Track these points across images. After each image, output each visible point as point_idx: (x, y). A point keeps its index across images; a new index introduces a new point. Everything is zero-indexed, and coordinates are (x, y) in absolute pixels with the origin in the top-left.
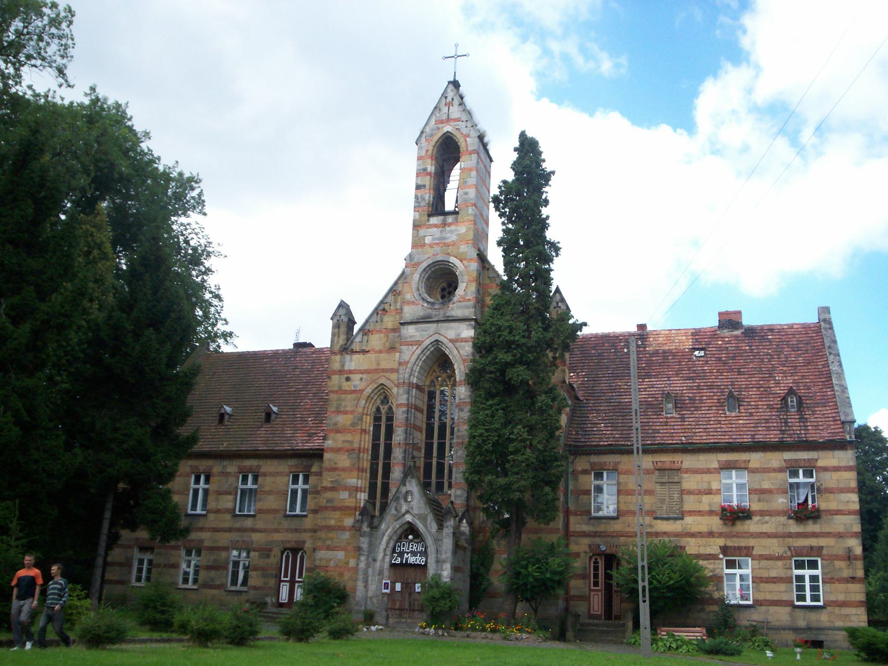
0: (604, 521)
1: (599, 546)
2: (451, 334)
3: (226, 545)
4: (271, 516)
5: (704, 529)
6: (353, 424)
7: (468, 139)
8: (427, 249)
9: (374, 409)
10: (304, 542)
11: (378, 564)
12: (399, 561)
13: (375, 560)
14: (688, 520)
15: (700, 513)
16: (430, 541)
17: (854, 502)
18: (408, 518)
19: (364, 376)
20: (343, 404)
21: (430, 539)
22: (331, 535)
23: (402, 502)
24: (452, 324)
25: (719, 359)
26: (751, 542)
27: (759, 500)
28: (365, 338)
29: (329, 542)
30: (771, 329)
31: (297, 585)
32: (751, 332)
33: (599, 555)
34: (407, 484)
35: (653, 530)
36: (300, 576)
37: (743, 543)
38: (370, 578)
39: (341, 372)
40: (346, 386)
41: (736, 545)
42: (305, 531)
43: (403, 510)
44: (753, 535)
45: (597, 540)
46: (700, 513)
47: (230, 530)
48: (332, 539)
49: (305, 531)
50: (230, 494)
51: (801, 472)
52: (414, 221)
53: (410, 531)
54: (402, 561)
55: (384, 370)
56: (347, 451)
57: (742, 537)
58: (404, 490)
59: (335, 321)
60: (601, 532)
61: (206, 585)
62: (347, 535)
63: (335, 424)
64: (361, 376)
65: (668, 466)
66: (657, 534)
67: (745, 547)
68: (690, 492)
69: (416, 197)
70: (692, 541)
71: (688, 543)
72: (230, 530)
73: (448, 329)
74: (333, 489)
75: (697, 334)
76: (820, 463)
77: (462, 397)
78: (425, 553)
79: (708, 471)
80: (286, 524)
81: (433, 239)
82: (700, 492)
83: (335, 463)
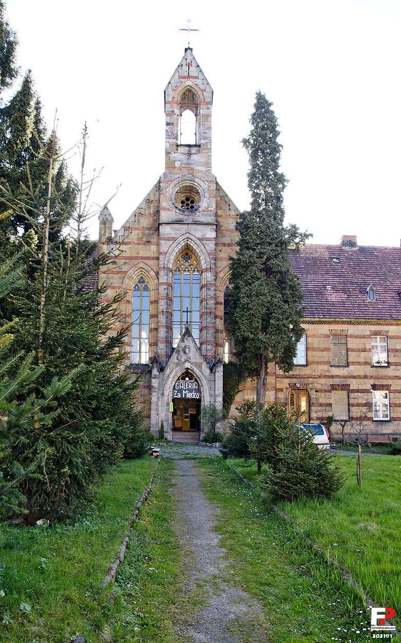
0: (298, 367)
1: (295, 384)
2: (199, 235)
5: (362, 374)
7: (204, 93)
8: (176, 171)
9: (225, 288)
11: (166, 398)
12: (179, 396)
13: (163, 395)
14: (352, 367)
15: (359, 363)
16: (204, 382)
18: (188, 365)
21: (204, 380)
23: (182, 353)
24: (199, 227)
25: (350, 265)
26: (389, 382)
27: (394, 356)
30: (375, 249)
32: (363, 250)
34: (185, 341)
35: (330, 374)
37: (385, 382)
38: (160, 408)
41: (381, 383)
43: (183, 360)
44: (390, 378)
45: (294, 381)
46: (359, 363)
52: (166, 149)
53: (188, 374)
54: (182, 395)
55: (142, 258)
57: (383, 379)
58: (183, 345)
59: (101, 219)
60: (297, 375)
64: (125, 261)
65: (339, 332)
66: (332, 377)
67: (386, 385)
68: (353, 350)
69: (167, 131)
70: (354, 381)
71: (352, 382)
75: (329, 248)
76: (350, 333)
77: (209, 280)
78: (198, 390)
79: (364, 337)
81: (182, 164)
82: (359, 350)
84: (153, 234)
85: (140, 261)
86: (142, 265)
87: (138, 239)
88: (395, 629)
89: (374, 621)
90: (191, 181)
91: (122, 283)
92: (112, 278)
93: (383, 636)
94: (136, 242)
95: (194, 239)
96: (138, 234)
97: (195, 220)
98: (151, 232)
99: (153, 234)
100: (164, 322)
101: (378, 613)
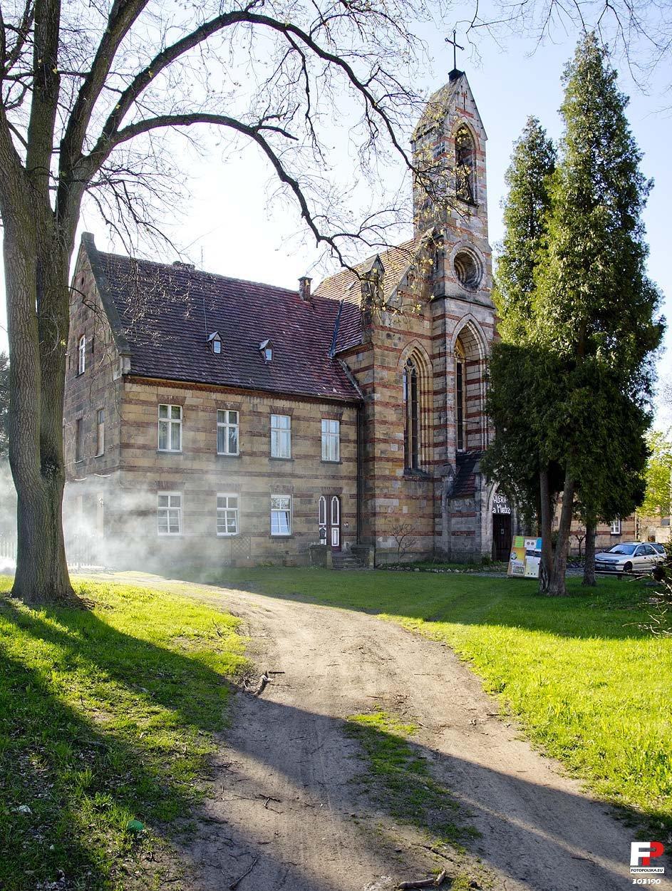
2: (480, 318)
10: (341, 488)
17: (393, 460)
19: (402, 336)
22: (387, 484)
29: (385, 491)
31: (332, 529)
36: (335, 521)
40: (388, 343)
42: (342, 478)
48: (388, 488)
49: (342, 478)
50: (265, 436)
51: (219, 424)
62: (399, 484)
63: (382, 379)
73: (477, 312)
74: (385, 441)
83: (385, 417)
86: (416, 344)
90: (470, 248)
95: (476, 322)
97: (476, 299)
100: (453, 420)
101: (641, 850)
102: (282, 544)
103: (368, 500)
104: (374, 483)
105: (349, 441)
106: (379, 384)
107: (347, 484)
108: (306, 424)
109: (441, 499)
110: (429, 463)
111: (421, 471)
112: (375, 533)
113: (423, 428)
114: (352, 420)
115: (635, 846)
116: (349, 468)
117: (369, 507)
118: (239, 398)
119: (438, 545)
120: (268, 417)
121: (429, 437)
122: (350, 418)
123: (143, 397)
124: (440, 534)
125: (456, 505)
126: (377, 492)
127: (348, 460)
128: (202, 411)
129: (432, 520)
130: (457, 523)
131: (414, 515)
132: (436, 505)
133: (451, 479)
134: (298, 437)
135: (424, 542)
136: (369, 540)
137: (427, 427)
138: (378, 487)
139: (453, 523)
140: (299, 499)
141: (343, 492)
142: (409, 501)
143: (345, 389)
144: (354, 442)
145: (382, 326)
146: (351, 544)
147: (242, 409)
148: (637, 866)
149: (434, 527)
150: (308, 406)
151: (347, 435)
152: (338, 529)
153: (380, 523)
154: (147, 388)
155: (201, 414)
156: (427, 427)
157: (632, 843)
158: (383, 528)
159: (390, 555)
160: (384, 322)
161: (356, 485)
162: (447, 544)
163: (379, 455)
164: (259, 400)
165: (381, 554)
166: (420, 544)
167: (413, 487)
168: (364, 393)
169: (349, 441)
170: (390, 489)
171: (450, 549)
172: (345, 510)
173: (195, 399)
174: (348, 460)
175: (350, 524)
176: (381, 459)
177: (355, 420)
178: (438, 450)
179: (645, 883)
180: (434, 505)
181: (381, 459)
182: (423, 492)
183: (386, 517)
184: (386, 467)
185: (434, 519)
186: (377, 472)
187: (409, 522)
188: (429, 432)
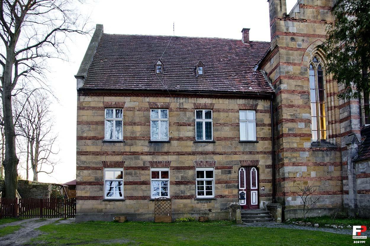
3: (192, 165)
4: (228, 143)
6: (301, 73)
19: (305, 38)
20: (291, 57)
22: (295, 154)
28: (302, 9)
29: (294, 160)
31: (252, 192)
33: (243, 167)
36: (254, 185)
39: (287, 34)
40: (292, 44)
42: (258, 153)
47: (194, 153)
48: (296, 157)
49: (258, 153)
50: (189, 125)
56: (300, 93)
61: (177, 197)
63: (288, 72)
64: (303, 38)
72: (194, 153)
74: (292, 121)
75: (270, 6)
80: (241, 148)
83: (291, 102)
84: (327, 13)
85: (317, 38)
87: (314, 17)
88: (366, 238)
89: (354, 233)
91: (302, 61)
92: (292, 55)
93: (360, 242)
94: (312, 19)
96: (313, 12)
98: (326, 11)
99: (327, 13)
101: (357, 229)
102: (206, 204)
103: (280, 168)
104: (283, 155)
105: (264, 125)
106: (285, 77)
107: (263, 157)
108: (225, 114)
109: (347, 164)
110: (336, 136)
111: (329, 143)
112: (284, 194)
113: (330, 109)
114: (266, 109)
115: (355, 227)
116: (266, 145)
117: (281, 174)
118: (168, 100)
119: (346, 202)
120: (192, 111)
121: (335, 115)
122: (264, 107)
123: (92, 105)
124: (347, 193)
125: (361, 167)
126: (286, 161)
127: (263, 139)
128: (137, 110)
129: (340, 182)
130: (363, 183)
131: (322, 178)
132: (343, 170)
133: (355, 146)
134: (219, 125)
135: (332, 200)
136: (281, 199)
137: (333, 108)
138: (287, 157)
139: (358, 183)
140: (220, 171)
141: (260, 164)
142: (317, 168)
143: (260, 87)
144: (269, 125)
145: (286, 33)
146: (267, 203)
147: (170, 107)
148: (355, 236)
149: (342, 188)
150: (226, 101)
151: (262, 120)
152: (257, 192)
153: (288, 186)
154: (96, 98)
155: (137, 113)
156: (333, 108)
157: (353, 226)
158: (293, 189)
159: (298, 211)
160: (287, 29)
161: (271, 158)
162: (353, 201)
163: (287, 132)
164: (184, 100)
165: (290, 211)
166: (327, 201)
167: (320, 156)
168: (275, 87)
169: (264, 125)
170: (298, 159)
171: (356, 205)
172: (262, 177)
173: (132, 103)
174: (263, 139)
175: (267, 188)
176: (288, 135)
177: (269, 109)
178: (343, 124)
179: (359, 243)
180: (342, 170)
181: (288, 135)
182: (331, 159)
183: (294, 181)
184: (294, 141)
185: (342, 181)
186: (285, 145)
187: (318, 184)
188: (335, 111)
